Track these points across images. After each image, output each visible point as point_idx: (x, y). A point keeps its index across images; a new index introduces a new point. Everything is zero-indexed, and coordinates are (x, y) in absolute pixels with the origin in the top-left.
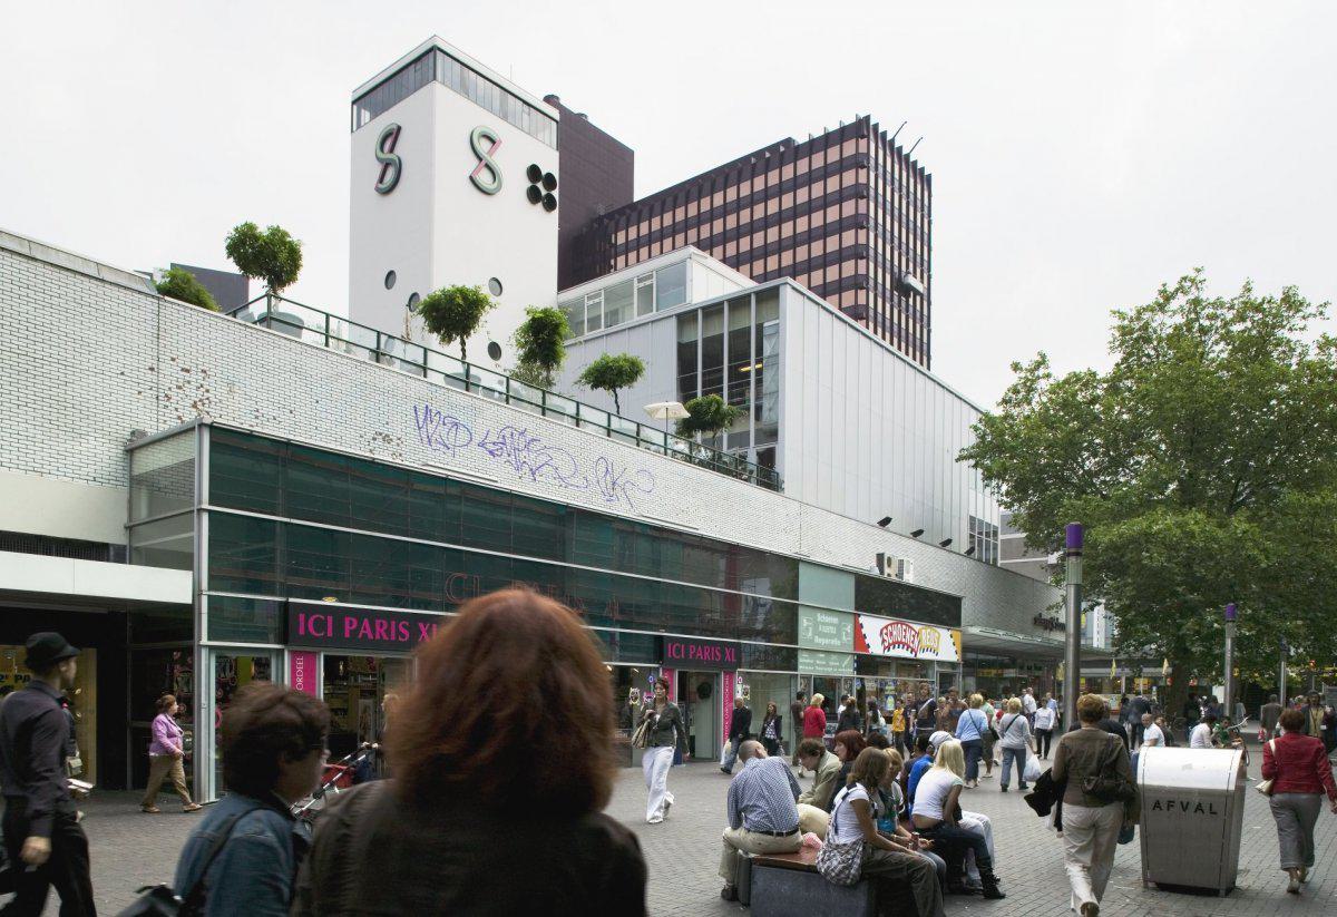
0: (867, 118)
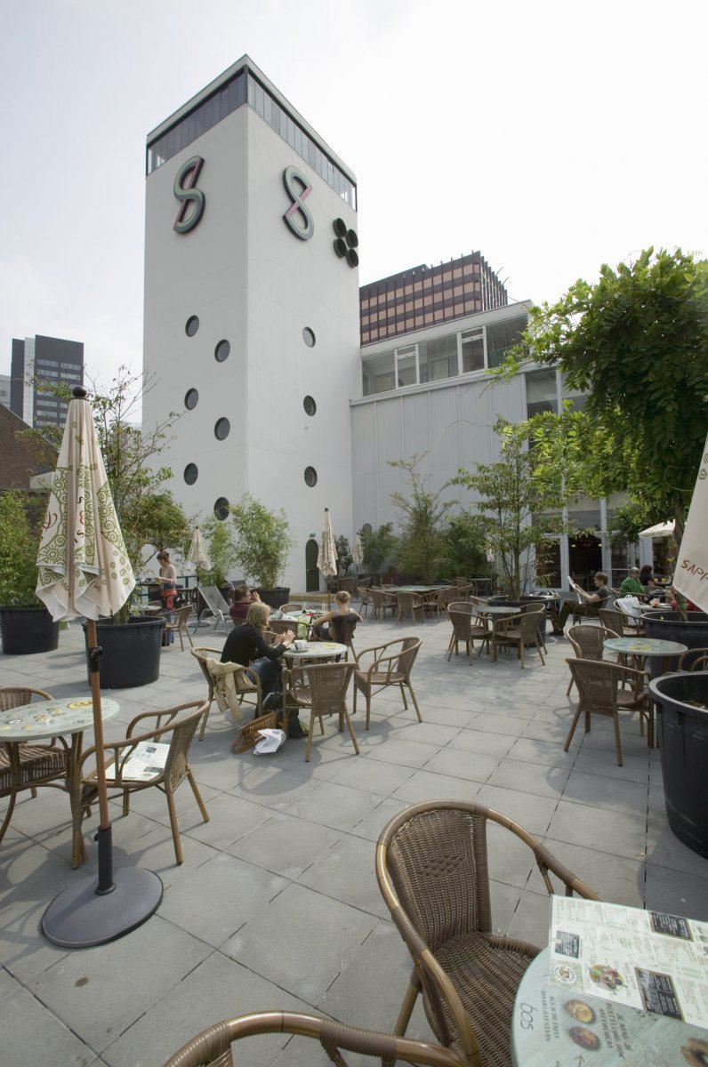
0: (478, 253)
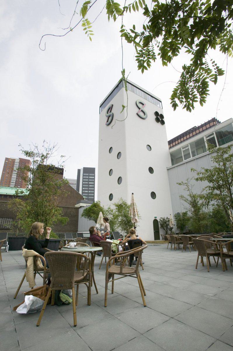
0: (214, 118)
